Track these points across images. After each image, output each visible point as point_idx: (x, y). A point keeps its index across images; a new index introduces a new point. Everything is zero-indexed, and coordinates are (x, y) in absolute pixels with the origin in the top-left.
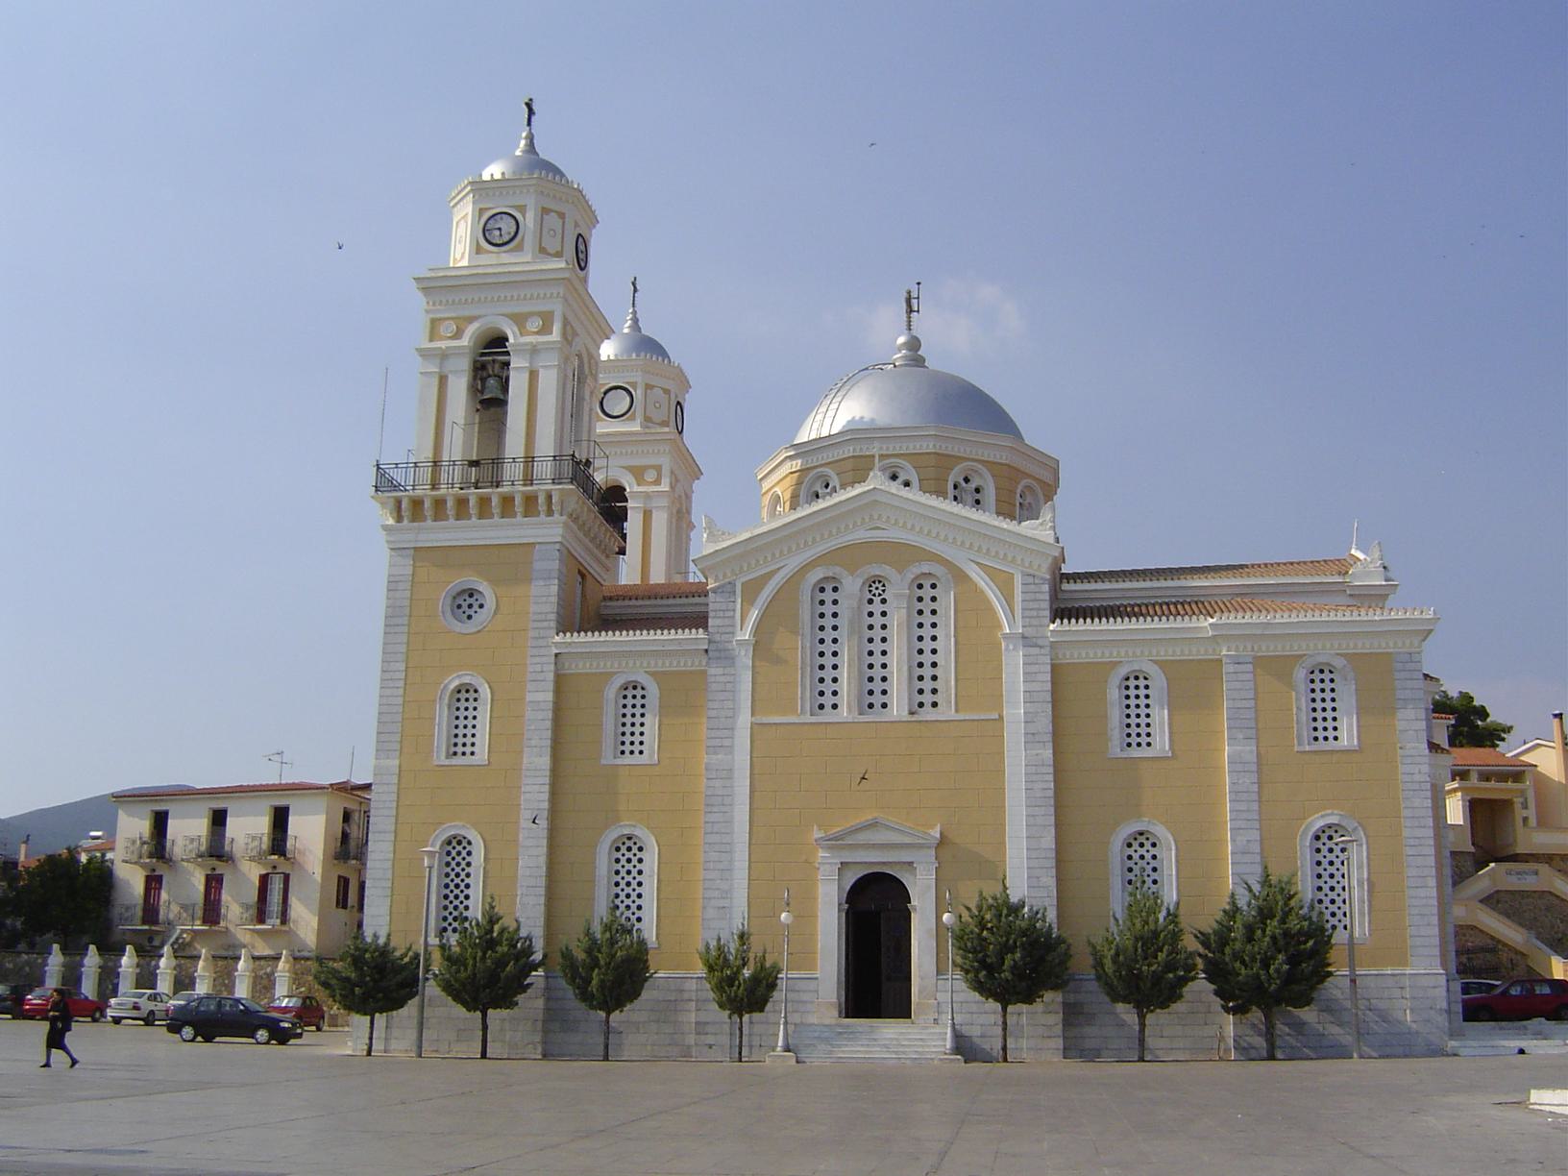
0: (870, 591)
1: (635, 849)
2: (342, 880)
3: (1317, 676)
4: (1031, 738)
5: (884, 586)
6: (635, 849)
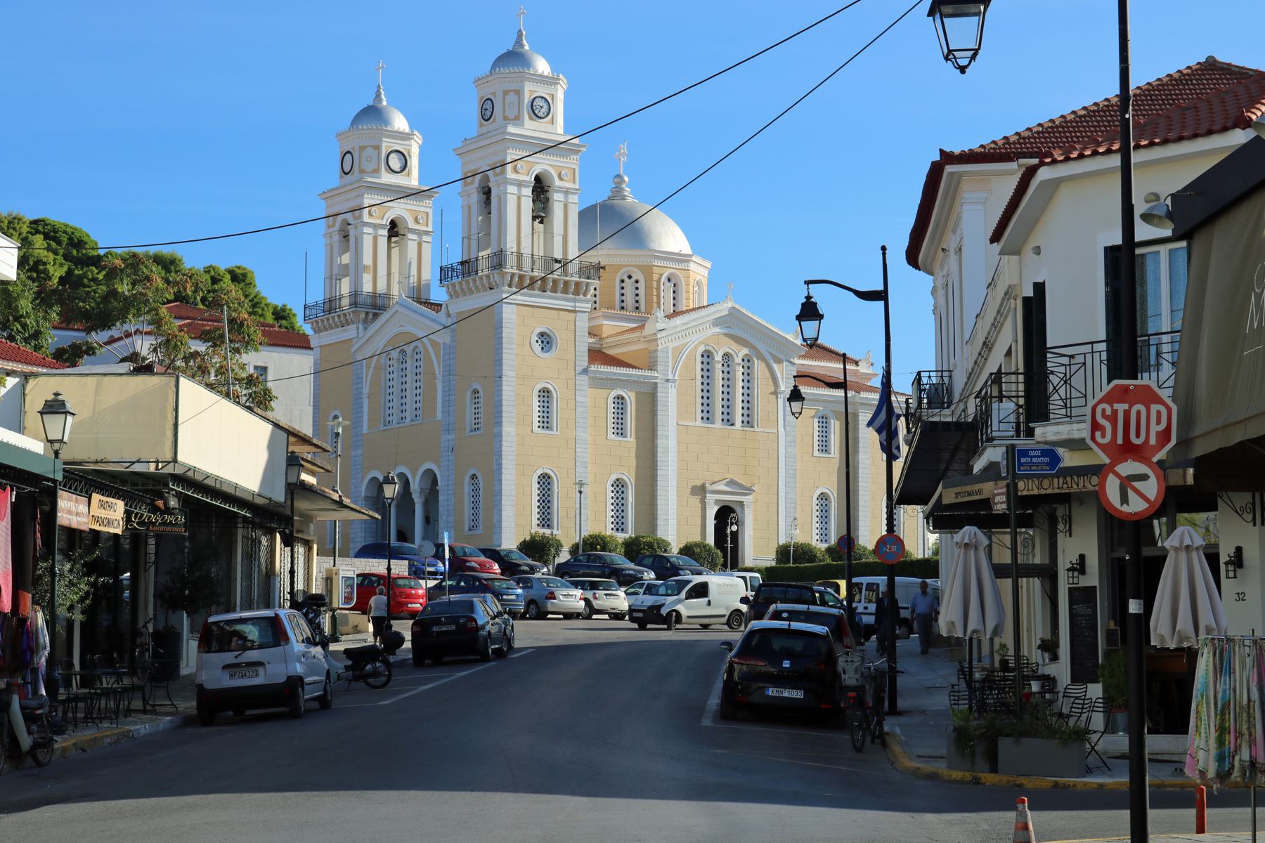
1: (620, 486)
3: (542, 394)
4: (667, 449)
6: (620, 486)
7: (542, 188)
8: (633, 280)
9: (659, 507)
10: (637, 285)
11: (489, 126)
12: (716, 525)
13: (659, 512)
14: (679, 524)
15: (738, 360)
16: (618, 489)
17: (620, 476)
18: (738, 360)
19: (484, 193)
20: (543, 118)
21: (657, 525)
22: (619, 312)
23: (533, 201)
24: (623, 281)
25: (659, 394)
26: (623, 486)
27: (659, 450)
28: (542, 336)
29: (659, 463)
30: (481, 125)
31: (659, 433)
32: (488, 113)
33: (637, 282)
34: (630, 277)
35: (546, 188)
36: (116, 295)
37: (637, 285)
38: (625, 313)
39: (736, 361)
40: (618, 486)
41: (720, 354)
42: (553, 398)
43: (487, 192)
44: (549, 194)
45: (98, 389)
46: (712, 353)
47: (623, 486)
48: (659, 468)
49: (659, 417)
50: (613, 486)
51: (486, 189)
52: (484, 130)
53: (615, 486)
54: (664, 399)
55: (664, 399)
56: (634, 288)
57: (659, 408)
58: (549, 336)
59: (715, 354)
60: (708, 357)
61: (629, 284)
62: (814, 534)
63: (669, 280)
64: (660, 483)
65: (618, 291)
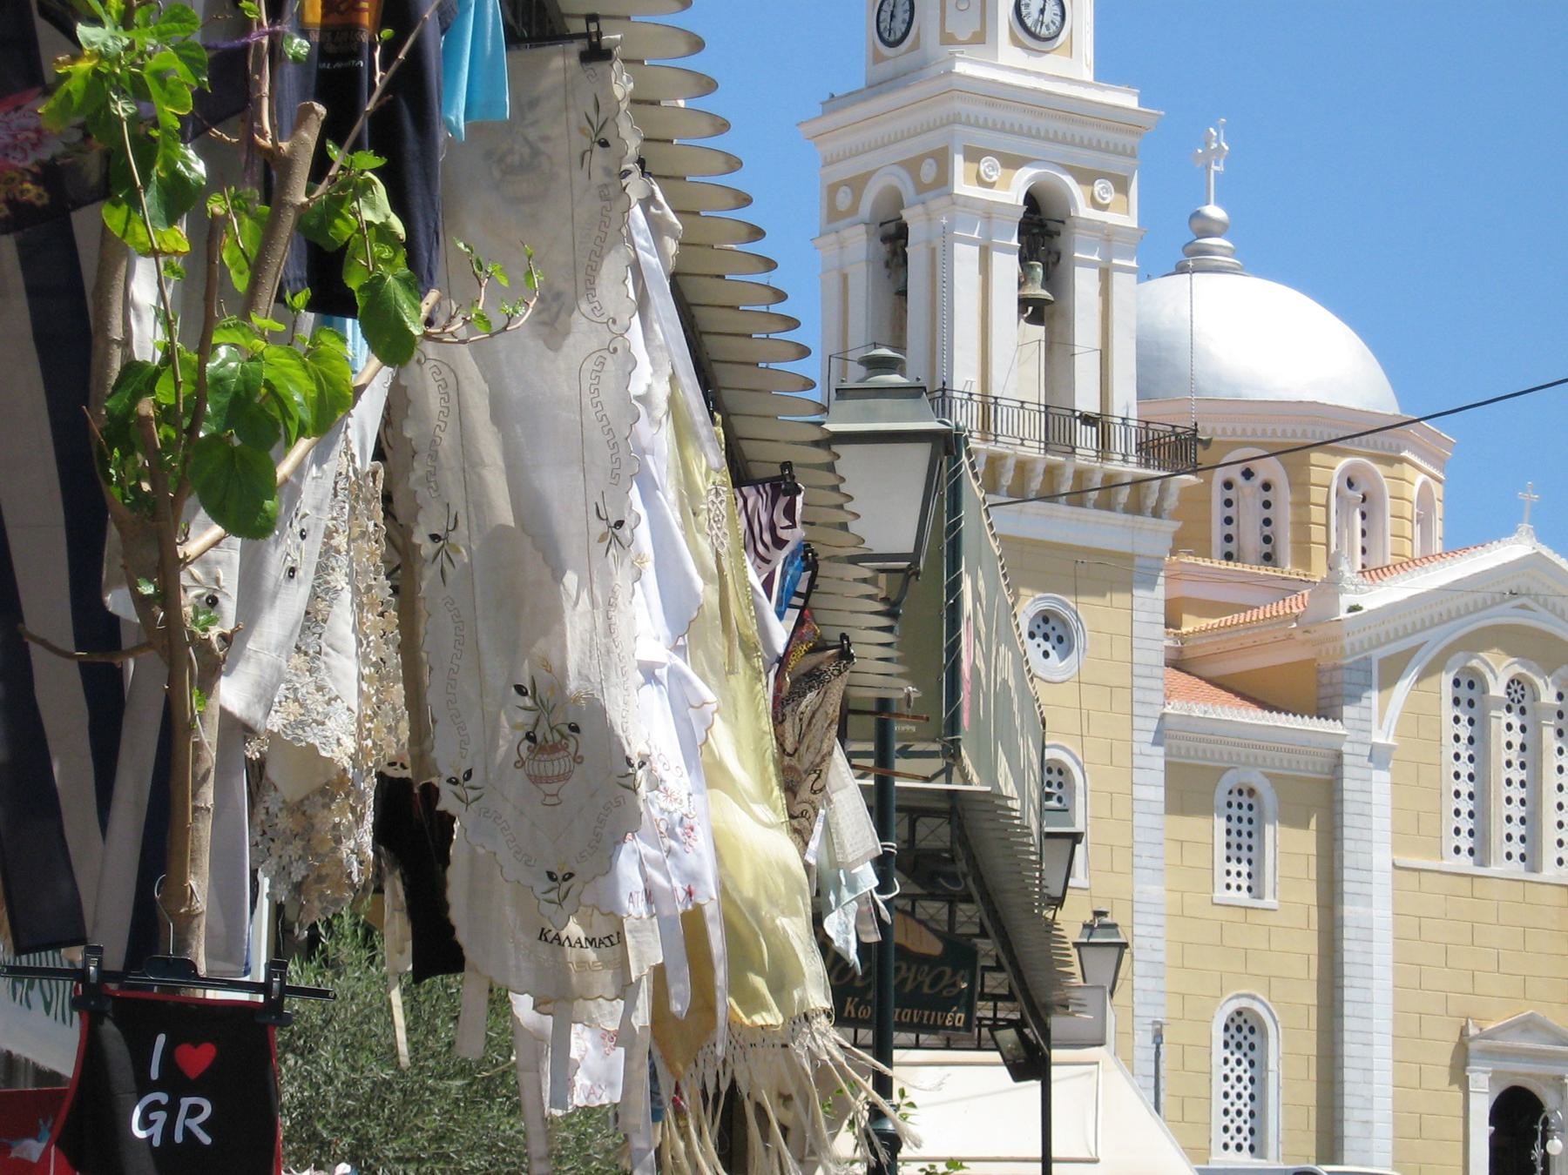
0: (1509, 694)
1: (1246, 1031)
2: (1151, 501)
5: (1523, 689)
6: (1246, 1031)
7: (1042, 225)
8: (1257, 481)
9: (1348, 1088)
10: (1268, 496)
11: (897, 58)
12: (1494, 1140)
13: (1348, 1101)
14: (1398, 1136)
15: (1497, 689)
16: (1239, 1037)
17: (1244, 1003)
18: (1497, 689)
19: (885, 239)
20: (1057, 35)
21: (1342, 1137)
22: (1255, 569)
23: (1021, 261)
24: (1228, 485)
25: (1347, 784)
26: (1252, 1030)
27: (1347, 933)
28: (1046, 620)
29: (1347, 970)
30: (878, 58)
31: (1347, 887)
32: (899, 27)
33: (1267, 486)
34: (1248, 474)
35: (1052, 226)
36: (1484, 693)
37: (1268, 496)
38: (1239, 567)
39: (1492, 693)
40: (1239, 1029)
41: (1504, 680)
42: (1073, 788)
43: (895, 237)
44: (1060, 242)
45: (1138, 960)
46: (1482, 678)
47: (1252, 1030)
48: (1346, 982)
49: (1348, 845)
50: (1227, 1028)
51: (891, 228)
52: (885, 69)
53: (1233, 1030)
54: (1358, 796)
55: (1358, 796)
56: (1259, 504)
57: (1347, 820)
58: (1064, 623)
59: (1489, 677)
60: (1471, 685)
61: (1248, 493)
62: (1217, 1077)
63: (1350, 484)
64: (1349, 1023)
65: (1217, 511)
